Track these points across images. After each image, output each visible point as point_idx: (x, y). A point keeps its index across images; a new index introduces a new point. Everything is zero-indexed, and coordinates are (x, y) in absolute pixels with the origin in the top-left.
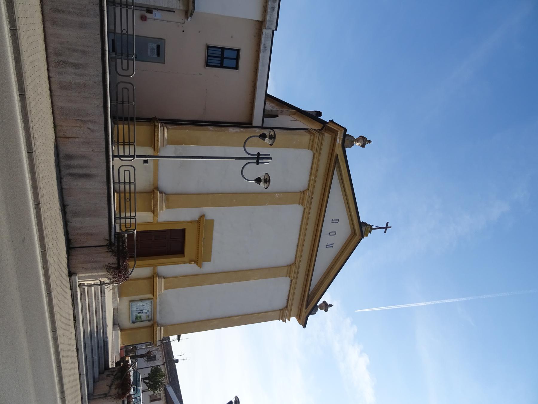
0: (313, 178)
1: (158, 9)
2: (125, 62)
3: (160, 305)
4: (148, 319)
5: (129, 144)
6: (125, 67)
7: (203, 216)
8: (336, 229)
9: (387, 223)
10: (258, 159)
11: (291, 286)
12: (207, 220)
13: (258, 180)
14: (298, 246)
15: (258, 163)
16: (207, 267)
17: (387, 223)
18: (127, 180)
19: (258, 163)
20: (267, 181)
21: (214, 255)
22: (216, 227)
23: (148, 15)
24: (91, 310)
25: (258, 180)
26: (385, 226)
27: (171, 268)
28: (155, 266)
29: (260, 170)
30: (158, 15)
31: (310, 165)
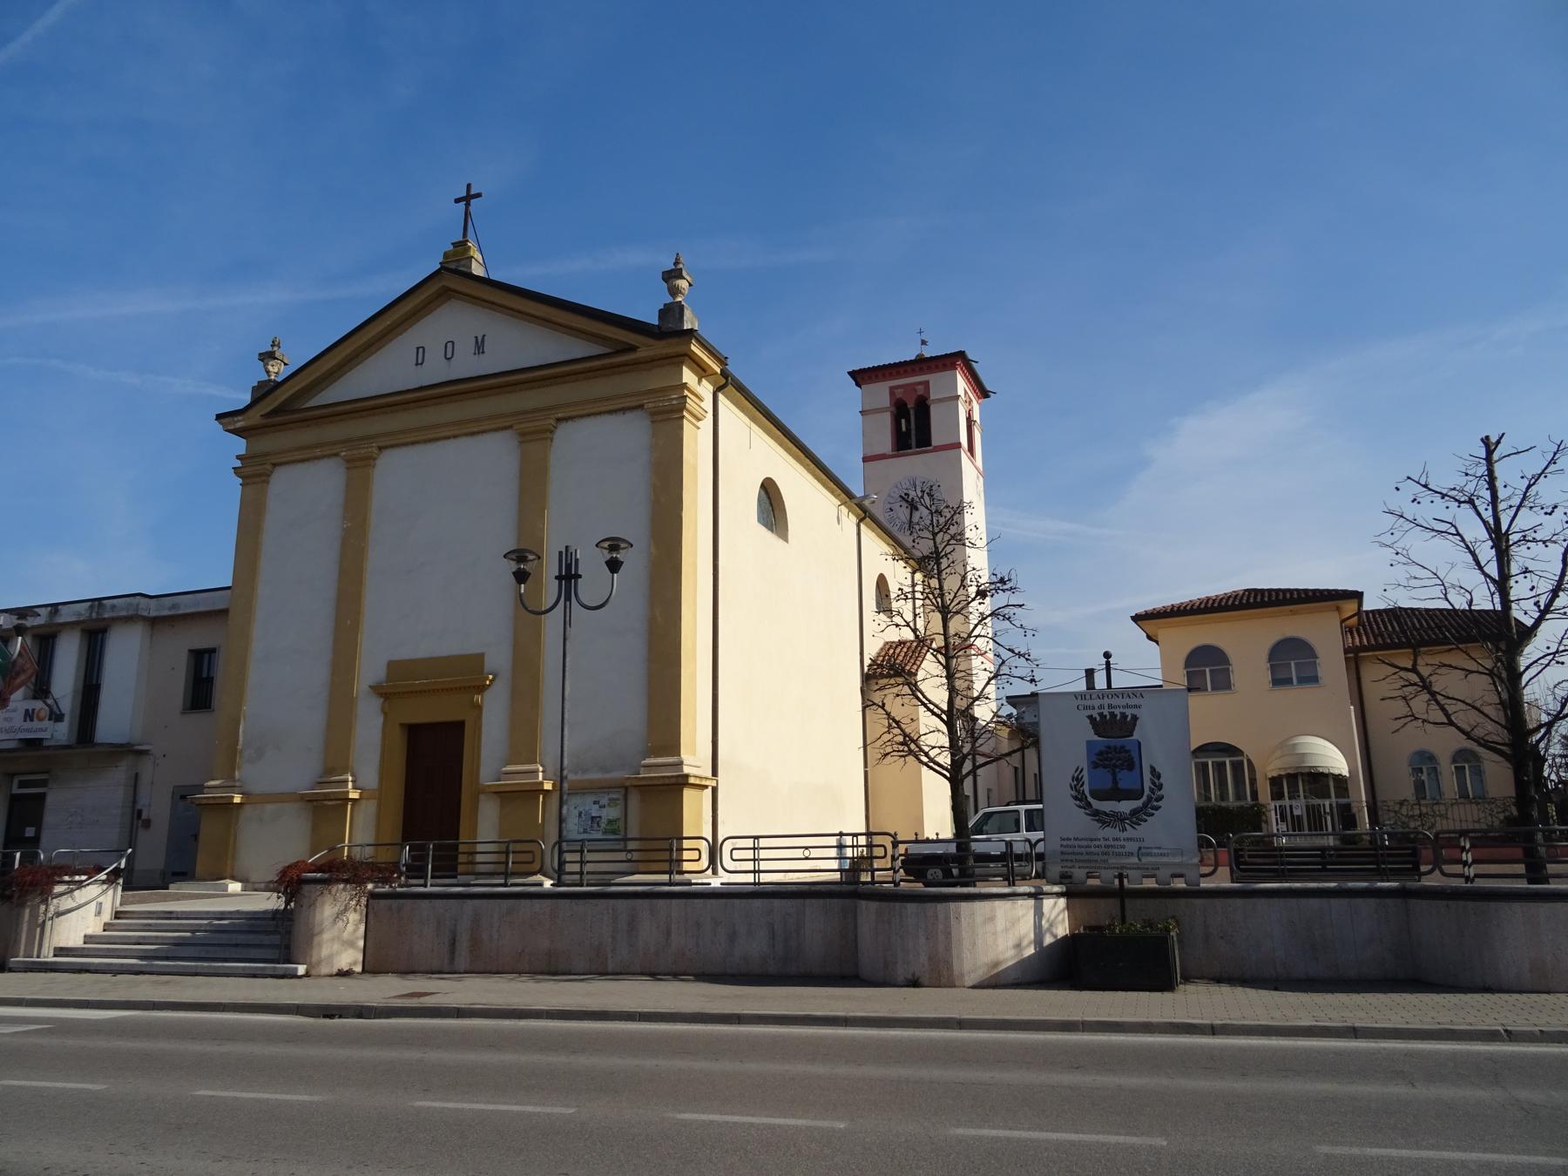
0: (318, 452)
1: (134, 802)
2: (686, 855)
3: (585, 771)
4: (621, 802)
5: (1415, 853)
6: (695, 855)
7: (379, 691)
8: (453, 344)
9: (469, 186)
10: (569, 577)
11: (582, 416)
12: (389, 677)
13: (614, 566)
14: (472, 434)
15: (559, 578)
16: (498, 659)
17: (469, 186)
18: (763, 854)
19: (559, 578)
20: (614, 544)
21: (471, 648)
22: (405, 653)
23: (144, 816)
24: (754, 947)
25: (614, 566)
26: (464, 194)
27: (490, 757)
28: (479, 791)
29: (591, 563)
30: (142, 802)
31: (300, 466)
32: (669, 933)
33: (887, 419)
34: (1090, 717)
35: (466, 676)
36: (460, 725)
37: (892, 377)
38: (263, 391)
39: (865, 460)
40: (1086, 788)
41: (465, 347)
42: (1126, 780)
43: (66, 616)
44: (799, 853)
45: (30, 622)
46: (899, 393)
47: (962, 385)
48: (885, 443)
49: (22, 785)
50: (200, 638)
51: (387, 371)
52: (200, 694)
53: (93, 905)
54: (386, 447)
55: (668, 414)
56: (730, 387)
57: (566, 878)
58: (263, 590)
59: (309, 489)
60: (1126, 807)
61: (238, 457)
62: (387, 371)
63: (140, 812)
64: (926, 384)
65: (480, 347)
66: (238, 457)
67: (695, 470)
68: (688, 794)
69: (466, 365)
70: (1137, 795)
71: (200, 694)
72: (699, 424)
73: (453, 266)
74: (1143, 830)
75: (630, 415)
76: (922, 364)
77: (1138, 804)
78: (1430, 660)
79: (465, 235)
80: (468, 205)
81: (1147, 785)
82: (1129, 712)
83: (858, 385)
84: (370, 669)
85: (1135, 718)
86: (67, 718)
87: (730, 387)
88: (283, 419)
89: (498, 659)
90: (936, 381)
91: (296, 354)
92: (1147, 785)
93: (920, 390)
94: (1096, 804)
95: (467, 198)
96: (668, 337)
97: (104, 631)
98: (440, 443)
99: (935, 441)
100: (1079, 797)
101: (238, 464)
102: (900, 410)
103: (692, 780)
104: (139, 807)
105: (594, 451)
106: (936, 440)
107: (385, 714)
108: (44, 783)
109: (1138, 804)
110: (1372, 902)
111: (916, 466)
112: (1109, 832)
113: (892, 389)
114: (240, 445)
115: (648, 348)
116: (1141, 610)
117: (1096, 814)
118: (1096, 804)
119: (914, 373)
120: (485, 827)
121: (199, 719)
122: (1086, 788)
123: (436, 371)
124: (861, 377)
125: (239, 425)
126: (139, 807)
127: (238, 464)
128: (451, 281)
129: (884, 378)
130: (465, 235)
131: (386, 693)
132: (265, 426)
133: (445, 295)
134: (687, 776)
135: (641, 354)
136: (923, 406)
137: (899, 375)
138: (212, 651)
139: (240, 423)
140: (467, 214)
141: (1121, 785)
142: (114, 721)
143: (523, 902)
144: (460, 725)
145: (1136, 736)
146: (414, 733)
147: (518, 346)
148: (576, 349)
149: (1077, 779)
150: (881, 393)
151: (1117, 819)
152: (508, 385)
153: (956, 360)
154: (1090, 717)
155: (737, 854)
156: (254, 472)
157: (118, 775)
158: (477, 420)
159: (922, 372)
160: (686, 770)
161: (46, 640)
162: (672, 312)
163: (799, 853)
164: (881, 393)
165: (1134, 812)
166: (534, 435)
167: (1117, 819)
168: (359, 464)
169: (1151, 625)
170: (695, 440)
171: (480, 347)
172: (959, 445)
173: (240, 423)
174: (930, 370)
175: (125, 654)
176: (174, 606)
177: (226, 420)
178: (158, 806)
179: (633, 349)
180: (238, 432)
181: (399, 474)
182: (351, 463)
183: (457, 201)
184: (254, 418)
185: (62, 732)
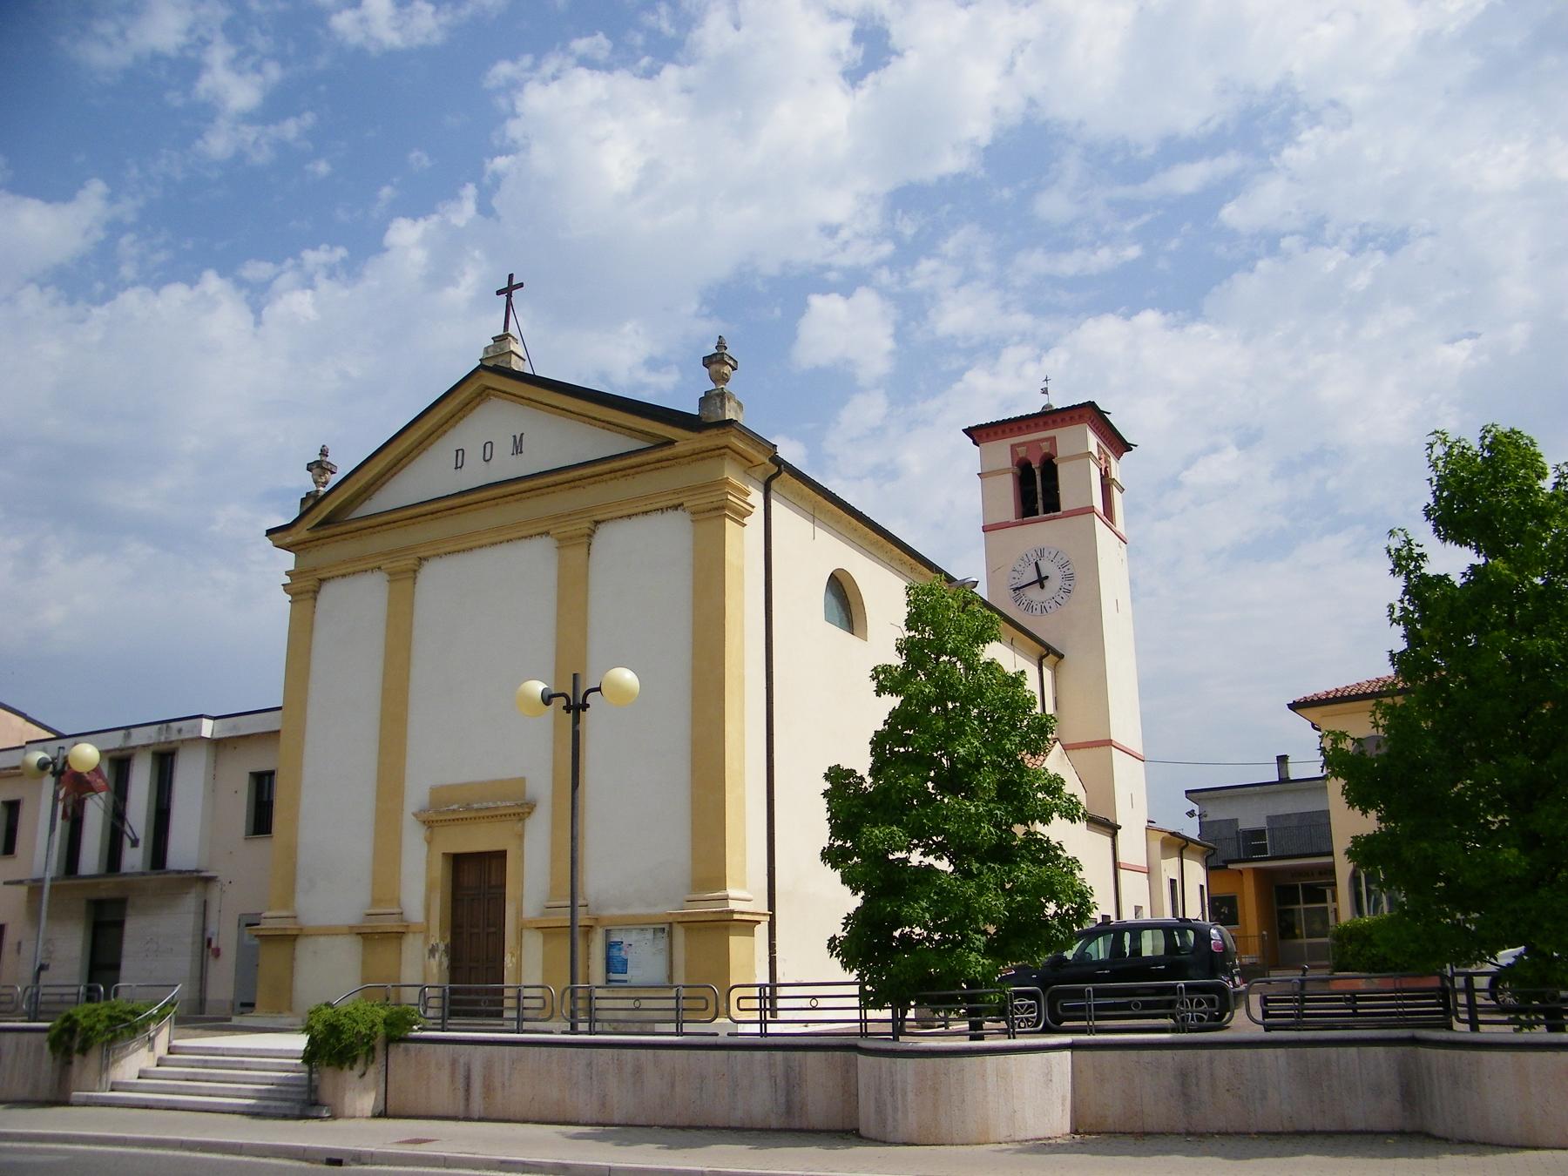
1: (204, 930)
8: (500, 443)
9: (511, 276)
17: (511, 276)
24: (760, 1102)
27: (531, 887)
30: (212, 928)
32: (673, 1086)
36: (502, 855)
37: (1012, 433)
38: (311, 502)
39: (985, 529)
41: (504, 447)
43: (139, 738)
44: (823, 1003)
46: (1022, 452)
47: (1093, 442)
52: (261, 820)
54: (426, 559)
56: (784, 475)
57: (598, 1027)
58: (313, 713)
59: (358, 601)
61: (287, 573)
63: (210, 941)
64: (1053, 440)
65: (518, 447)
66: (287, 573)
69: (506, 466)
71: (261, 820)
72: (746, 520)
73: (490, 364)
75: (671, 514)
76: (1050, 417)
78: (1094, 874)
79: (506, 327)
80: (509, 297)
83: (975, 443)
84: (416, 796)
86: (141, 844)
87: (784, 475)
88: (336, 524)
89: (542, 782)
91: (344, 463)
93: (1046, 448)
95: (508, 291)
99: (1065, 505)
101: (287, 580)
104: (208, 935)
105: (638, 553)
107: (429, 843)
111: (1043, 533)
113: (1013, 447)
114: (288, 560)
115: (687, 441)
116: (1298, 697)
119: (1037, 428)
120: (529, 964)
121: (261, 844)
123: (476, 474)
124: (977, 434)
125: (289, 540)
126: (208, 935)
127: (287, 580)
128: (497, 376)
129: (1004, 436)
130: (506, 327)
131: (432, 822)
133: (484, 394)
134: (733, 912)
135: (679, 448)
136: (1050, 468)
137: (1020, 431)
138: (271, 774)
139: (302, 533)
140: (509, 305)
142: (183, 850)
144: (502, 855)
146: (458, 862)
147: (558, 442)
150: (1002, 452)
155: (743, 1003)
156: (304, 590)
157: (190, 903)
159: (1046, 427)
160: (733, 905)
163: (805, 1003)
164: (1002, 452)
166: (578, 537)
168: (405, 575)
169: (1315, 713)
170: (742, 542)
171: (518, 447)
172: (1091, 510)
174: (1055, 425)
175: (190, 778)
177: (278, 535)
178: (226, 935)
179: (671, 442)
180: (287, 548)
181: (441, 581)
182: (394, 576)
183: (499, 293)
184: (302, 533)
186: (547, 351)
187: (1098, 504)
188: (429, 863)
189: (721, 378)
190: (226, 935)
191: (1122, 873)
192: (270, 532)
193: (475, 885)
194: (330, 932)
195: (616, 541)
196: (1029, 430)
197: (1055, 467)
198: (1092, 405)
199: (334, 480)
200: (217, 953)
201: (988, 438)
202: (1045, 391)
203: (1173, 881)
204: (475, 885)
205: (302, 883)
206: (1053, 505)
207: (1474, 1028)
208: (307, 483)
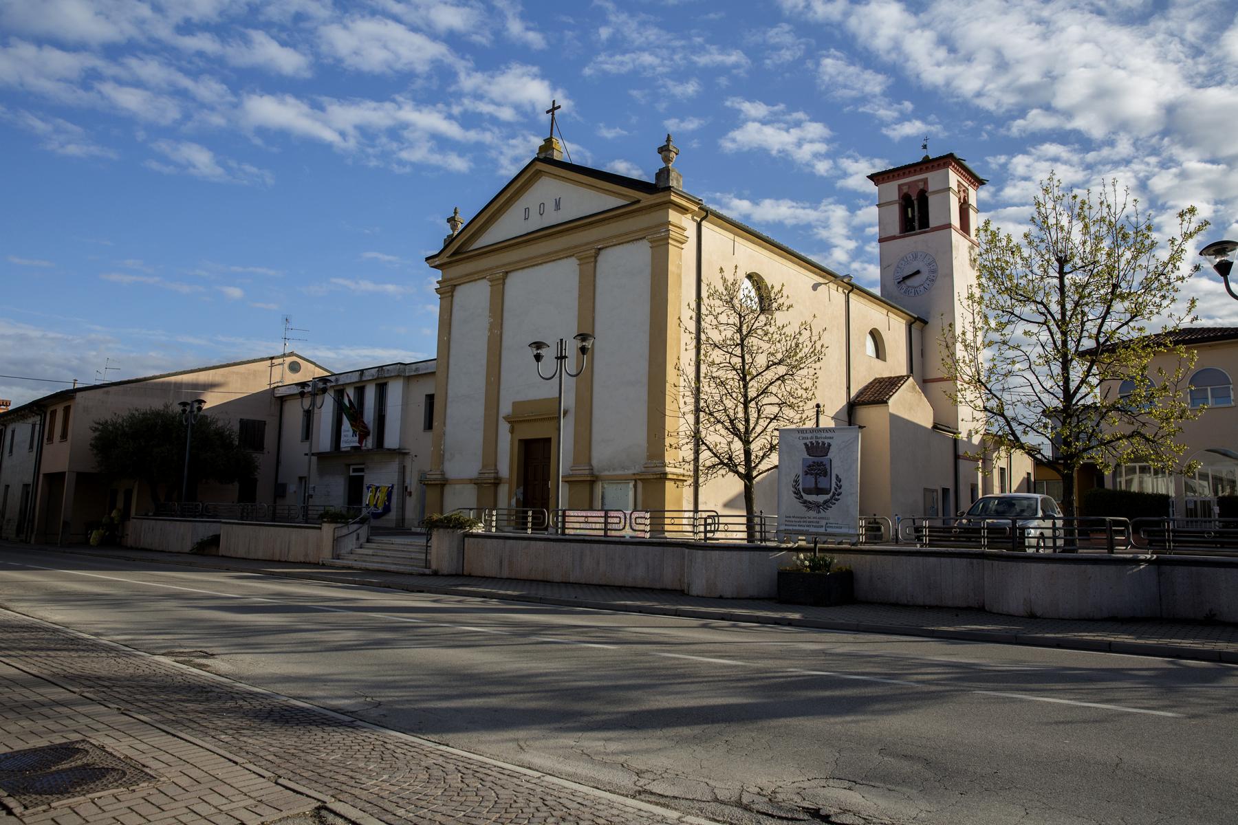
0: (476, 277)
20: (538, 345)
25: (538, 358)
27: (565, 459)
30: (407, 481)
32: (598, 564)
33: (896, 209)
34: (806, 444)
35: (551, 413)
36: (548, 441)
37: (899, 177)
38: (450, 241)
40: (800, 487)
41: (550, 206)
42: (823, 483)
43: (367, 377)
45: (307, 390)
46: (905, 190)
47: (954, 178)
48: (895, 229)
49: (355, 470)
50: (428, 387)
51: (509, 226)
53: (355, 535)
55: (660, 241)
59: (474, 296)
60: (821, 498)
62: (509, 226)
64: (925, 181)
65: (558, 206)
67: (679, 276)
68: (669, 486)
70: (826, 492)
74: (829, 513)
76: (928, 164)
77: (827, 497)
81: (834, 485)
82: (826, 441)
84: (506, 408)
85: (829, 445)
90: (933, 179)
91: (464, 219)
92: (834, 485)
93: (921, 186)
94: (806, 497)
96: (654, 192)
97: (386, 384)
98: (526, 271)
100: (797, 493)
102: (906, 201)
103: (670, 476)
105: (623, 263)
106: (933, 222)
108: (362, 470)
109: (827, 497)
110: (965, 561)
112: (812, 514)
113: (900, 187)
114: (437, 275)
115: (646, 199)
117: (805, 502)
118: (806, 497)
119: (915, 173)
122: (800, 487)
123: (535, 223)
128: (546, 159)
129: (894, 178)
131: (513, 422)
132: (450, 263)
133: (538, 174)
136: (923, 198)
137: (904, 175)
139: (437, 262)
141: (820, 486)
142: (391, 441)
143: (533, 543)
144: (548, 441)
145: (830, 455)
147: (585, 201)
148: (611, 202)
149: (796, 481)
150: (892, 190)
151: (817, 506)
152: (572, 228)
153: (948, 160)
154: (806, 444)
156: (447, 291)
157: (394, 466)
158: (556, 252)
159: (921, 171)
161: (360, 391)
162: (664, 174)
165: (826, 502)
166: (590, 258)
167: (817, 506)
171: (558, 206)
172: (949, 226)
173: (437, 262)
174: (927, 170)
176: (417, 369)
179: (638, 201)
180: (435, 267)
182: (582, 261)
184: (444, 259)
185: (369, 443)
186: (566, 150)
187: (955, 220)
188: (512, 444)
189: (667, 160)
190: (412, 482)
191: (961, 462)
192: (427, 259)
193: (535, 457)
194: (462, 481)
195: (612, 260)
196: (910, 174)
197: (927, 199)
198: (951, 156)
199: (460, 227)
200: (410, 494)
201: (884, 181)
202: (925, 147)
203: (1002, 469)
204: (535, 457)
205: (447, 456)
206: (924, 223)
207: (1111, 551)
208: (447, 230)
